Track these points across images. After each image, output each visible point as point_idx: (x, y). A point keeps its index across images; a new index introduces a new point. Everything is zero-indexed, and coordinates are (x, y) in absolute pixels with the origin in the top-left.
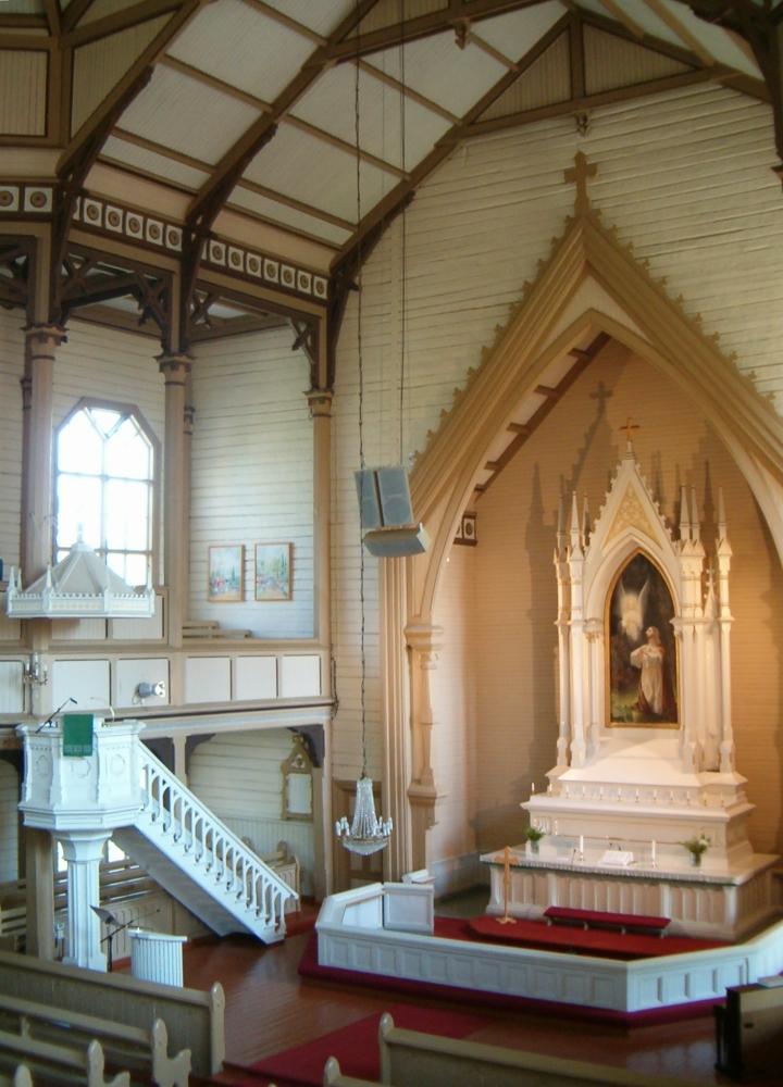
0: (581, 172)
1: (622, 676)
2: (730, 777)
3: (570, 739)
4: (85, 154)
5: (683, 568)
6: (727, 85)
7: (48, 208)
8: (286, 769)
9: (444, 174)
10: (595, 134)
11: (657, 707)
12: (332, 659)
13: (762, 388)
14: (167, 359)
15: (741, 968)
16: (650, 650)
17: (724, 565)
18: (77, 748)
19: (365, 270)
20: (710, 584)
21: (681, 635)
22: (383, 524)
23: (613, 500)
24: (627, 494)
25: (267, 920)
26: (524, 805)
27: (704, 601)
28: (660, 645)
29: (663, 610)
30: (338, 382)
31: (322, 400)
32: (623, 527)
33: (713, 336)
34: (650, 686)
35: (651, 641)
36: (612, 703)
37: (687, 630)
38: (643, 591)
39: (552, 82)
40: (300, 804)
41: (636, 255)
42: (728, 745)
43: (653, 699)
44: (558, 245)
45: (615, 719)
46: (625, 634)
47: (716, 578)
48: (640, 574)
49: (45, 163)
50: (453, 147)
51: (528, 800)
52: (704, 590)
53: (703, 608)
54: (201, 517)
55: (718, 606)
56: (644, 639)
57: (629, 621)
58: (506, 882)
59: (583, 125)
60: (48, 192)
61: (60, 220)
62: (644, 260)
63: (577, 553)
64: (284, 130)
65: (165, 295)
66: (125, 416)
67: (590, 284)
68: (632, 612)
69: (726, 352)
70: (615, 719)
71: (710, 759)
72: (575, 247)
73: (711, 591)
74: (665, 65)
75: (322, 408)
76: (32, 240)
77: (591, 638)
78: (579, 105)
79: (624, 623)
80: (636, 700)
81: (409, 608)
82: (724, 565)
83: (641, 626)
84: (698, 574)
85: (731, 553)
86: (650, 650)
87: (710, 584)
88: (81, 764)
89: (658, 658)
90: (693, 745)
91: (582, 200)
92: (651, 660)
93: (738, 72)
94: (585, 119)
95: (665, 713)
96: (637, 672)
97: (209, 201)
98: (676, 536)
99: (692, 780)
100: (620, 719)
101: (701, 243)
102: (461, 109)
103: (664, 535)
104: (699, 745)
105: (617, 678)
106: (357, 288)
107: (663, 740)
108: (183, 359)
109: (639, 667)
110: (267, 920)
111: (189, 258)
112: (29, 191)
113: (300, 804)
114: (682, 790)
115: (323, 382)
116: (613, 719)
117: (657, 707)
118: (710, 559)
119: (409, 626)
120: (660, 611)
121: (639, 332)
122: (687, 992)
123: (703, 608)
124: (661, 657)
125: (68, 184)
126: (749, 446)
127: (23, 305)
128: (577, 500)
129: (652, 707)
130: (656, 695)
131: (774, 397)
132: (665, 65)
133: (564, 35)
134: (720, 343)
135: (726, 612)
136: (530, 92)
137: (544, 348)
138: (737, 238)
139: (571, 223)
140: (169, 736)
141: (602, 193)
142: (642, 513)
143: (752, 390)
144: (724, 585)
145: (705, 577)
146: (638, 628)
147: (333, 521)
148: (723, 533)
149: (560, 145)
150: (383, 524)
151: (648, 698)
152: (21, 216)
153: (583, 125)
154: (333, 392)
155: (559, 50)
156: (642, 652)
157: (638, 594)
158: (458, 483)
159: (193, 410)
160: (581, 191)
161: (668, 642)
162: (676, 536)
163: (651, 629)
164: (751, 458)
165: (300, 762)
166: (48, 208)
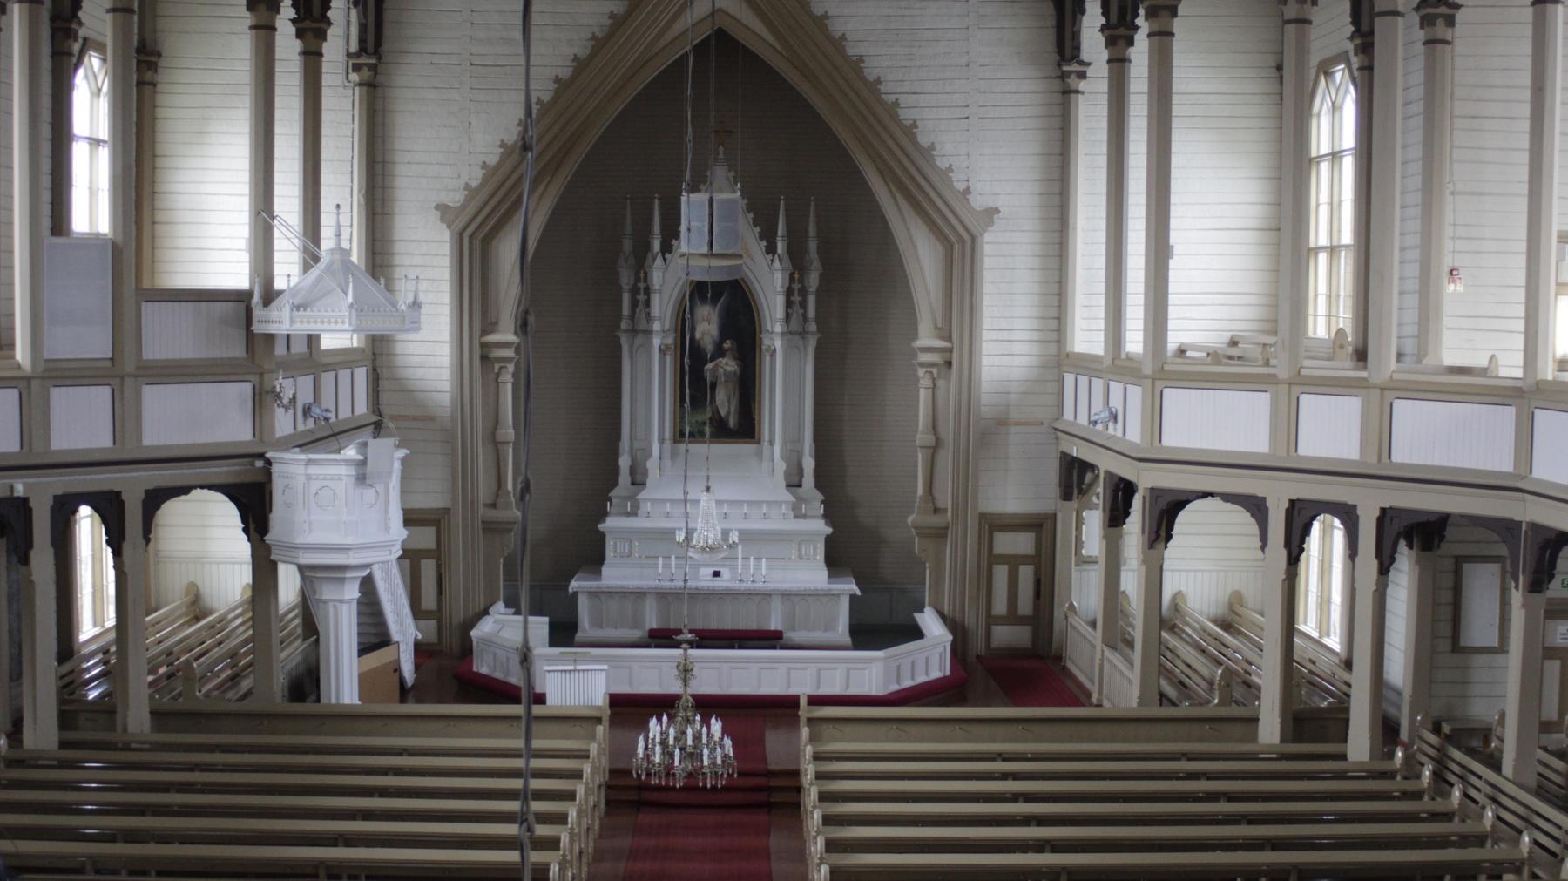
11: (732, 423)
12: (374, 370)
13: (923, 140)
14: (308, 24)
15: (941, 654)
16: (727, 364)
20: (796, 298)
28: (739, 359)
30: (386, 47)
33: (822, 16)
34: (725, 402)
35: (727, 353)
38: (720, 302)
41: (850, 52)
43: (728, 413)
46: (699, 347)
47: (804, 292)
51: (604, 521)
54: (164, 193)
56: (719, 352)
57: (703, 334)
62: (911, 122)
63: (659, 261)
68: (707, 326)
69: (871, 77)
86: (727, 364)
89: (735, 372)
98: (771, 249)
117: (732, 423)
122: (927, 674)
124: (738, 371)
126: (886, 173)
129: (728, 421)
130: (732, 409)
131: (863, 62)
134: (883, 88)
137: (662, 43)
140: (116, 489)
143: (894, 117)
146: (714, 342)
147: (379, 210)
151: (723, 413)
154: (380, 58)
156: (717, 365)
157: (716, 306)
158: (549, 182)
163: (728, 341)
164: (889, 186)
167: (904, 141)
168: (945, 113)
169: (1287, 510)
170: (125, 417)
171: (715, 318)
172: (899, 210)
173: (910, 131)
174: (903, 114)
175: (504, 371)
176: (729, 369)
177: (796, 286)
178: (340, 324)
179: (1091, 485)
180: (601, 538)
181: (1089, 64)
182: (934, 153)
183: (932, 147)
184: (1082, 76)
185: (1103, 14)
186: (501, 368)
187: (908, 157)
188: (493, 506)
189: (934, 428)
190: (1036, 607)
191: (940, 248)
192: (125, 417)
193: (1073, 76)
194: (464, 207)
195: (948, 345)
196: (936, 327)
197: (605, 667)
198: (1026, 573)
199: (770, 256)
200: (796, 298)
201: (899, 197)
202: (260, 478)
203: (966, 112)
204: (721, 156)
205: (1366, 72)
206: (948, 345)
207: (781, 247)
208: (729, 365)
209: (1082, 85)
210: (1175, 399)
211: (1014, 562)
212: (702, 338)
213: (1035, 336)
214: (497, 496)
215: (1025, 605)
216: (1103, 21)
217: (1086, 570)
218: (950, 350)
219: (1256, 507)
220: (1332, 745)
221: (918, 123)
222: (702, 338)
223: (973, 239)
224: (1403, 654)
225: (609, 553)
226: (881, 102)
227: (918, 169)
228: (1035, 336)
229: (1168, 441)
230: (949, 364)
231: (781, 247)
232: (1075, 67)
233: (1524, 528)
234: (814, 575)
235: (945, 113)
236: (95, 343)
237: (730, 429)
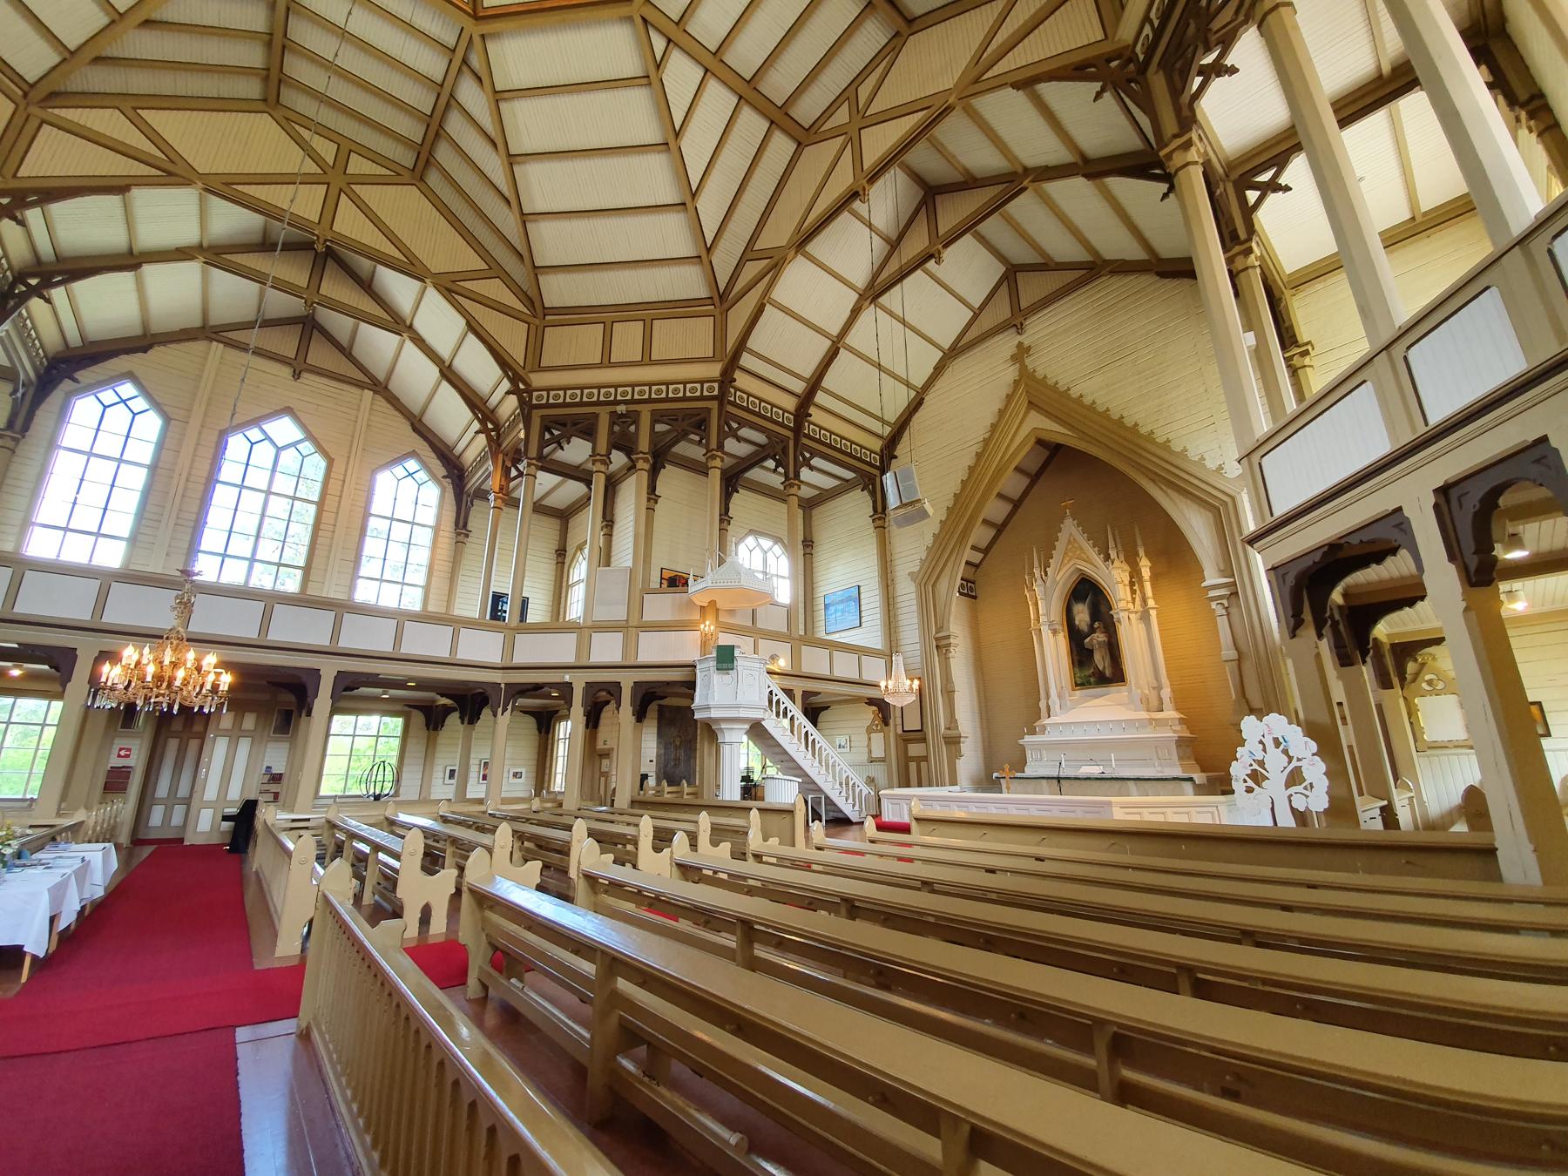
0: (1021, 353)
1: (1080, 654)
2: (1170, 713)
3: (1048, 697)
4: (732, 364)
5: (1114, 578)
7: (716, 393)
8: (869, 731)
9: (940, 384)
17: (1146, 573)
18: (725, 665)
19: (899, 447)
21: (1119, 621)
23: (1060, 545)
24: (1069, 541)
25: (854, 806)
26: (1021, 741)
27: (1134, 599)
31: (880, 518)
32: (1069, 561)
34: (1101, 660)
37: (1123, 615)
39: (1001, 310)
40: (878, 752)
42: (1166, 693)
43: (1104, 667)
44: (1009, 398)
45: (1080, 684)
48: (1086, 591)
49: (715, 370)
52: (1133, 592)
53: (1134, 603)
55: (1144, 601)
56: (1092, 630)
58: (1007, 783)
59: (1020, 329)
60: (716, 385)
61: (721, 398)
63: (1040, 581)
64: (843, 354)
65: (785, 451)
66: (776, 543)
67: (1033, 414)
68: (1082, 615)
71: (1154, 703)
72: (1021, 394)
73: (1138, 592)
74: (1071, 276)
75: (879, 523)
76: (709, 410)
77: (1055, 632)
78: (1015, 323)
79: (1077, 623)
80: (1092, 670)
81: (936, 623)
82: (1146, 573)
84: (1127, 582)
85: (1149, 564)
87: (1136, 587)
88: (727, 678)
90: (1139, 691)
91: (1023, 368)
92: (1099, 643)
93: (1117, 260)
94: (1022, 324)
95: (1114, 676)
96: (1091, 652)
97: (806, 401)
98: (1107, 558)
99: (1144, 715)
101: (1106, 369)
102: (946, 345)
103: (1098, 560)
104: (1143, 692)
105: (1076, 658)
107: (1115, 693)
109: (1090, 648)
110: (854, 806)
111: (797, 430)
112: (706, 385)
113: (878, 752)
115: (880, 509)
116: (1077, 685)
117: (1108, 673)
118: (1135, 575)
119: (937, 633)
121: (1067, 432)
123: (1134, 603)
124: (1106, 640)
125: (726, 379)
126: (1156, 478)
132: (1071, 276)
133: (1005, 283)
135: (1151, 603)
136: (986, 322)
138: (1129, 359)
139: (1016, 383)
141: (1034, 363)
142: (1081, 549)
145: (1132, 584)
148: (1141, 552)
149: (1006, 343)
151: (1101, 668)
152: (702, 398)
153: (1020, 329)
155: (1004, 288)
161: (1110, 628)
162: (1107, 558)
164: (1162, 489)
165: (877, 725)
166: (716, 393)
167: (1166, 456)
168: (1195, 427)
169: (1436, 507)
170: (630, 646)
172: (1170, 498)
173: (1166, 446)
174: (1143, 431)
179: (1416, 675)
180: (1023, 750)
182: (1155, 436)
183: (1185, 450)
187: (1150, 453)
188: (949, 729)
189: (1235, 645)
191: (1210, 515)
192: (630, 646)
194: (920, 571)
195: (1232, 580)
196: (1220, 571)
197: (800, 780)
201: (1170, 491)
202: (692, 679)
206: (1232, 580)
208: (1100, 637)
209: (1307, 361)
214: (951, 723)
217: (1434, 755)
218: (1234, 584)
220: (1381, 877)
223: (1233, 499)
224: (1543, 522)
225: (1029, 759)
226: (1140, 436)
227: (1177, 467)
231: (1113, 554)
235: (1195, 427)
236: (620, 613)
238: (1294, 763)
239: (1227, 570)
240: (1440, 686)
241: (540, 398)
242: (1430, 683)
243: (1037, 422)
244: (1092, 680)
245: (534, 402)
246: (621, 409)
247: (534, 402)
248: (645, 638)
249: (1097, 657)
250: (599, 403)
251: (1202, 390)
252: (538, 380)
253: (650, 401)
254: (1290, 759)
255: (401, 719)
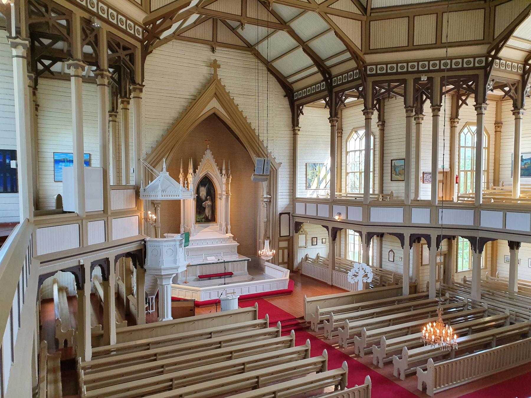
2: (229, 235)
6: (255, 54)
10: (216, 54)
22: (263, 173)
29: (212, 192)
34: (208, 212)
36: (197, 217)
42: (229, 227)
45: (197, 222)
47: (228, 184)
50: (171, 40)
56: (206, 200)
57: (202, 195)
67: (214, 99)
68: (203, 192)
70: (197, 222)
79: (201, 195)
80: (204, 216)
83: (206, 196)
95: (212, 219)
96: (205, 208)
100: (199, 222)
106: (285, 96)
107: (212, 226)
108: (336, 118)
114: (224, 239)
117: (210, 218)
120: (212, 193)
122: (249, 292)
127: (84, 53)
128: (225, 164)
141: (221, 73)
144: (230, 185)
150: (263, 173)
152: (474, 68)
159: (38, 106)
160: (215, 71)
171: (205, 190)
175: (158, 206)
176: (209, 204)
177: (186, 182)
178: (164, 197)
181: (300, 127)
184: (299, 130)
185: (431, 103)
186: (157, 206)
190: (288, 260)
193: (297, 130)
198: (286, 251)
199: (221, 174)
200: (186, 185)
203: (273, 138)
204: (208, 147)
205: (499, 120)
207: (224, 172)
208: (209, 203)
209: (422, 122)
210: (484, 214)
211: (283, 249)
212: (202, 196)
213: (288, 194)
215: (286, 260)
216: (405, 106)
219: (401, 237)
221: (264, 141)
222: (202, 196)
223: (276, 170)
228: (288, 194)
229: (372, 220)
230: (270, 201)
231: (224, 172)
232: (298, 128)
233: (478, 238)
234: (236, 257)
237: (209, 220)
238: (366, 273)
239: (269, 193)
240: (303, 232)
241: (371, 70)
242: (302, 232)
243: (214, 105)
244: (203, 220)
245: (368, 72)
246: (446, 74)
247: (368, 72)
248: (484, 214)
249: (207, 211)
250: (408, 73)
251: (272, 125)
252: (369, 59)
253: (440, 70)
254: (365, 272)
255: (287, 242)
